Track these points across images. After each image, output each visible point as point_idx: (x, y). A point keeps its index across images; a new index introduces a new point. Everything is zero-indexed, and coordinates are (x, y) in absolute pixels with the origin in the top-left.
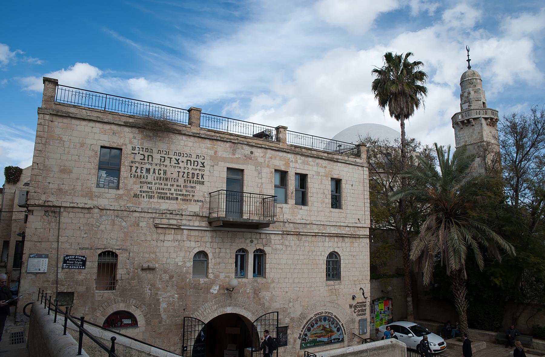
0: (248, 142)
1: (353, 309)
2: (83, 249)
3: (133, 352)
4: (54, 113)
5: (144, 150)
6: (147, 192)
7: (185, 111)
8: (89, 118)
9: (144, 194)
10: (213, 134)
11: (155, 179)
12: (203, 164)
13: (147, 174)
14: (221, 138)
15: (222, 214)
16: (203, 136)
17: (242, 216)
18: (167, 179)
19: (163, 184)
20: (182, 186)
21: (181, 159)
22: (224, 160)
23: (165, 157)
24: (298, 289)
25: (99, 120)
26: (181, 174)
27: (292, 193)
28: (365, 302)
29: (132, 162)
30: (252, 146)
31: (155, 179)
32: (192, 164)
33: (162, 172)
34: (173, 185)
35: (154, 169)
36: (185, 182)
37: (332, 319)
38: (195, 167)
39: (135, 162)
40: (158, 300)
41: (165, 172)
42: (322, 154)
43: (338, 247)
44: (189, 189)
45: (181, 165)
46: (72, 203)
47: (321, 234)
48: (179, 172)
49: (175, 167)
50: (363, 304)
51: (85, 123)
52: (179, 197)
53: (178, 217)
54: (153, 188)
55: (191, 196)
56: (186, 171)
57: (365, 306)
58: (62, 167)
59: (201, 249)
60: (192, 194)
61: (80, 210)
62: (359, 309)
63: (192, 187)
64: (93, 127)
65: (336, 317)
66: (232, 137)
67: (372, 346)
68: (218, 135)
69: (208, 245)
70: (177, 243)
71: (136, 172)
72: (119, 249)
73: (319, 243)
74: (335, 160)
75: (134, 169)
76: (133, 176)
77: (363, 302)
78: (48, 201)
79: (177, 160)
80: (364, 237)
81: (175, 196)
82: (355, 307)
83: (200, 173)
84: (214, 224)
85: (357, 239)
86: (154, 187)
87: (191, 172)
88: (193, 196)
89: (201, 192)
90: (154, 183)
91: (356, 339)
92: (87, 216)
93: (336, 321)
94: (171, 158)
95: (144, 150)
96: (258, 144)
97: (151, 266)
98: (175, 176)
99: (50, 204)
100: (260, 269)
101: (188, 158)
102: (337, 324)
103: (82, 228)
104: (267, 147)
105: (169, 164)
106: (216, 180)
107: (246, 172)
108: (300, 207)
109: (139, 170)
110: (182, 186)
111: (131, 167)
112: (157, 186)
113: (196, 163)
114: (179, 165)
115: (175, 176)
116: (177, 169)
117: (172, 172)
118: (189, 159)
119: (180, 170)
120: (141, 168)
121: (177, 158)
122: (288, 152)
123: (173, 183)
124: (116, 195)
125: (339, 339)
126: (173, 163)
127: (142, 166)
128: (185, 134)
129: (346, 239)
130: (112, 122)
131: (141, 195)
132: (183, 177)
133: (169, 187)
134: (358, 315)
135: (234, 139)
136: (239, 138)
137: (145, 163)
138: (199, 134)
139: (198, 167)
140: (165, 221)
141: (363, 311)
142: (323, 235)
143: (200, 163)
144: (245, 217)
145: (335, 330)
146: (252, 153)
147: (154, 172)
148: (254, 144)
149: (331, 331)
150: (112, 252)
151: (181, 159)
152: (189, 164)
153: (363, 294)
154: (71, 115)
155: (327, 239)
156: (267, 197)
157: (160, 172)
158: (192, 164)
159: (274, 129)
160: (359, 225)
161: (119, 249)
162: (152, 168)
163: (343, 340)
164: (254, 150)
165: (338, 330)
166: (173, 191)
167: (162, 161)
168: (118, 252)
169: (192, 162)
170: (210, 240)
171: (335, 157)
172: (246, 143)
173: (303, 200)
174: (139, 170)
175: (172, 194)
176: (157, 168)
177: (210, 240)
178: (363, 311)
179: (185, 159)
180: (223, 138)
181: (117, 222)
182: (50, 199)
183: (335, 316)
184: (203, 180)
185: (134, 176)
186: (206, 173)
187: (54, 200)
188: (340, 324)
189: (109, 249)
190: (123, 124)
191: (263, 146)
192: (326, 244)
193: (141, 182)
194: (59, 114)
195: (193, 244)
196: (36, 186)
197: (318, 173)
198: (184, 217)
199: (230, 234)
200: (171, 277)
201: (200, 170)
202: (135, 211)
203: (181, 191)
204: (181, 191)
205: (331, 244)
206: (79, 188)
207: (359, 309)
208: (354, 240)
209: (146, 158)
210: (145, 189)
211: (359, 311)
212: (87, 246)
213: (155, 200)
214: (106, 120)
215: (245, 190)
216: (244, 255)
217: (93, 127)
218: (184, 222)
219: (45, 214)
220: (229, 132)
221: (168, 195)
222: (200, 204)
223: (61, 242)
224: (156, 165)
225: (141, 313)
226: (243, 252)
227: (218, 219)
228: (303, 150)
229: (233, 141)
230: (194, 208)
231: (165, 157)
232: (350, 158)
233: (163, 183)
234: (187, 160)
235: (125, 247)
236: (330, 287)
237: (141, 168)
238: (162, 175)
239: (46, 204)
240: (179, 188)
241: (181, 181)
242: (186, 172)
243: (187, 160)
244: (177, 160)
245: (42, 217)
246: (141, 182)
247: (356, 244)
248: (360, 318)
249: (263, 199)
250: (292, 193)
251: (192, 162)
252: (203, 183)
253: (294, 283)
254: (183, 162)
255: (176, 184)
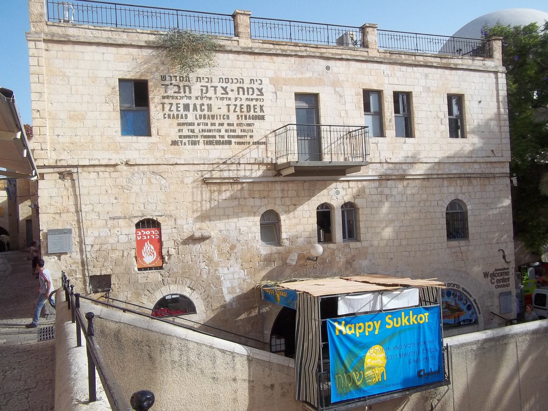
0: (321, 53)
1: (489, 278)
2: (114, 219)
3: (191, 346)
4: (49, 38)
5: (178, 78)
6: (189, 137)
7: (228, 18)
8: (97, 40)
9: (185, 140)
10: (271, 46)
11: (198, 117)
12: (260, 90)
13: (186, 113)
14: (283, 50)
15: (293, 158)
16: (256, 51)
17: (320, 158)
18: (213, 117)
19: (209, 124)
20: (235, 125)
21: (230, 86)
22: (287, 82)
23: (207, 87)
24: (407, 254)
25: (110, 42)
26: (232, 108)
27: (390, 121)
28: (508, 269)
29: (164, 97)
30: (328, 59)
31: (198, 117)
32: (246, 93)
33: (205, 107)
34: (222, 125)
35: (195, 105)
36: (238, 118)
37: (458, 294)
38: (250, 97)
39: (168, 97)
40: (218, 278)
41: (210, 107)
42: (432, 60)
43: (463, 194)
44: (246, 128)
45: (231, 95)
46: (92, 159)
47: (436, 177)
48: (228, 105)
49: (222, 99)
50: (504, 272)
51: (94, 48)
52: (233, 140)
53: (234, 167)
54: (196, 131)
55: (248, 137)
56: (238, 103)
57: (507, 274)
58: (72, 113)
59: (270, 208)
60: (250, 134)
61: (103, 169)
62: (499, 278)
63: (249, 125)
64: (104, 53)
65: (466, 291)
66: (298, 48)
67: (522, 330)
68: (277, 47)
69: (278, 201)
70: (236, 202)
71: (170, 110)
72: (161, 216)
73: (434, 189)
74: (452, 66)
75: (167, 107)
76: (166, 116)
77: (505, 269)
78: (60, 160)
79: (225, 89)
80: (502, 175)
81: (226, 138)
82: (493, 275)
83: (258, 103)
84: (285, 172)
85: (491, 180)
86: (196, 128)
87: (245, 103)
88: (251, 137)
89: (260, 129)
90: (196, 124)
91: (496, 320)
92: (115, 175)
93: (466, 296)
94: (215, 87)
95: (178, 78)
96: (336, 54)
97: (206, 234)
98: (224, 111)
99: (64, 163)
100: (351, 232)
101: (239, 85)
102: (467, 300)
103: (109, 191)
104: (349, 57)
105: (214, 96)
106: (281, 112)
107: (322, 98)
108: (403, 139)
109: (174, 108)
110: (235, 125)
111: (163, 104)
112: (201, 127)
113: (250, 90)
114: (228, 96)
115: (224, 111)
116: (226, 102)
117: (219, 107)
118: (241, 85)
119: (229, 102)
120: (177, 104)
121: (224, 85)
122: (381, 63)
123: (222, 121)
124: (148, 144)
125: (471, 320)
126: (219, 94)
127: (178, 101)
128: (231, 52)
129: (475, 182)
130: (129, 43)
131: (181, 142)
132: (235, 111)
133: (217, 127)
134: (498, 287)
135: (300, 51)
136: (308, 49)
137: (182, 98)
138: (251, 48)
139: (255, 96)
140: (216, 174)
141: (504, 280)
142: (440, 176)
143: (256, 90)
144: (327, 159)
145: (464, 308)
146: (328, 68)
147: (195, 109)
148: (330, 56)
149: (459, 310)
150: (152, 220)
151: (230, 86)
152: (241, 92)
153: (504, 257)
154: (72, 39)
155: (446, 183)
156: (354, 129)
157: (203, 107)
158: (246, 93)
159: (358, 30)
160: (493, 159)
161: (161, 216)
162: (191, 102)
163: (476, 322)
164: (331, 63)
165: (469, 308)
166: (223, 133)
167: (204, 91)
168: (160, 220)
169: (246, 90)
170: (280, 195)
171: (452, 61)
172: (318, 55)
173: (407, 129)
174: (174, 108)
175: (223, 137)
176: (198, 102)
177: (280, 195)
178: (504, 280)
179: (235, 86)
180: (286, 51)
181: (154, 181)
182: (62, 157)
183: (463, 289)
184: (262, 114)
185: (169, 116)
186: (266, 104)
187: (68, 159)
188: (472, 300)
189: (149, 217)
190: (143, 44)
191: (344, 57)
192: (445, 190)
193: (179, 124)
194: (55, 39)
195: (258, 202)
196: (42, 140)
197: (428, 89)
198: (242, 167)
199: (307, 185)
200: (233, 247)
201: (257, 100)
202: (176, 164)
203: (234, 131)
204: (234, 131)
205: (452, 190)
206: (98, 139)
207: (499, 278)
208: (486, 182)
209: (182, 90)
210: (185, 133)
211: (498, 281)
212: (119, 214)
213: (202, 146)
214: (120, 42)
215: (323, 121)
216: (352, 210)
217: (104, 53)
218: (242, 174)
219: (60, 178)
220: (293, 41)
221: (218, 138)
222: (263, 146)
223: (86, 212)
224: (197, 98)
225: (198, 296)
226: (327, 208)
227: (288, 165)
228: (403, 56)
229: (300, 54)
230: (256, 153)
231: (207, 87)
232: (476, 62)
233: (209, 122)
234: (238, 88)
235: (168, 213)
236: (453, 250)
237: (177, 104)
238: (206, 112)
239: (59, 164)
240: (232, 128)
241: (233, 118)
242: (239, 105)
243: (238, 88)
244: (225, 89)
245: (55, 181)
246: (179, 124)
247: (490, 188)
248: (500, 292)
249: (350, 132)
250: (390, 121)
251: (246, 90)
252: (262, 118)
253: (401, 245)
254: (232, 90)
255: (226, 122)
